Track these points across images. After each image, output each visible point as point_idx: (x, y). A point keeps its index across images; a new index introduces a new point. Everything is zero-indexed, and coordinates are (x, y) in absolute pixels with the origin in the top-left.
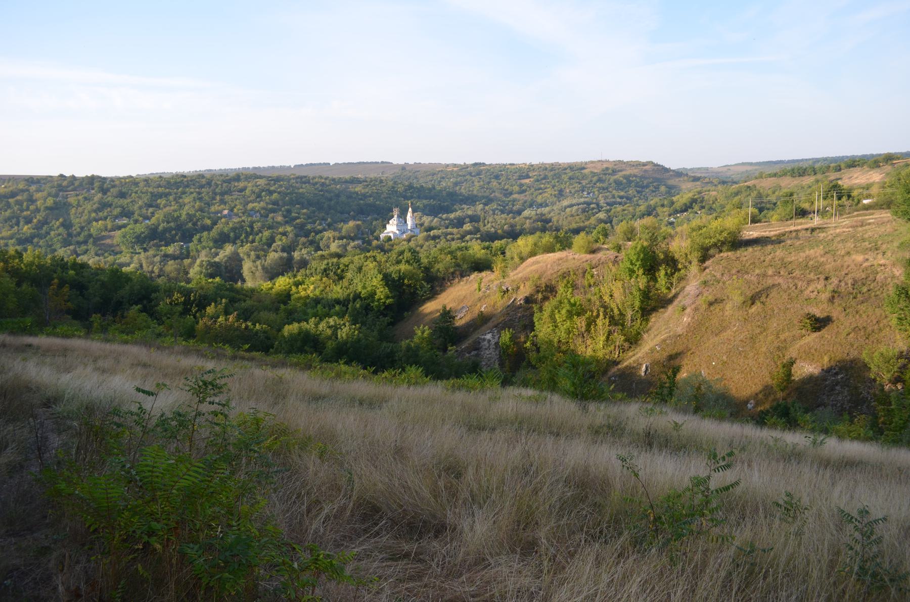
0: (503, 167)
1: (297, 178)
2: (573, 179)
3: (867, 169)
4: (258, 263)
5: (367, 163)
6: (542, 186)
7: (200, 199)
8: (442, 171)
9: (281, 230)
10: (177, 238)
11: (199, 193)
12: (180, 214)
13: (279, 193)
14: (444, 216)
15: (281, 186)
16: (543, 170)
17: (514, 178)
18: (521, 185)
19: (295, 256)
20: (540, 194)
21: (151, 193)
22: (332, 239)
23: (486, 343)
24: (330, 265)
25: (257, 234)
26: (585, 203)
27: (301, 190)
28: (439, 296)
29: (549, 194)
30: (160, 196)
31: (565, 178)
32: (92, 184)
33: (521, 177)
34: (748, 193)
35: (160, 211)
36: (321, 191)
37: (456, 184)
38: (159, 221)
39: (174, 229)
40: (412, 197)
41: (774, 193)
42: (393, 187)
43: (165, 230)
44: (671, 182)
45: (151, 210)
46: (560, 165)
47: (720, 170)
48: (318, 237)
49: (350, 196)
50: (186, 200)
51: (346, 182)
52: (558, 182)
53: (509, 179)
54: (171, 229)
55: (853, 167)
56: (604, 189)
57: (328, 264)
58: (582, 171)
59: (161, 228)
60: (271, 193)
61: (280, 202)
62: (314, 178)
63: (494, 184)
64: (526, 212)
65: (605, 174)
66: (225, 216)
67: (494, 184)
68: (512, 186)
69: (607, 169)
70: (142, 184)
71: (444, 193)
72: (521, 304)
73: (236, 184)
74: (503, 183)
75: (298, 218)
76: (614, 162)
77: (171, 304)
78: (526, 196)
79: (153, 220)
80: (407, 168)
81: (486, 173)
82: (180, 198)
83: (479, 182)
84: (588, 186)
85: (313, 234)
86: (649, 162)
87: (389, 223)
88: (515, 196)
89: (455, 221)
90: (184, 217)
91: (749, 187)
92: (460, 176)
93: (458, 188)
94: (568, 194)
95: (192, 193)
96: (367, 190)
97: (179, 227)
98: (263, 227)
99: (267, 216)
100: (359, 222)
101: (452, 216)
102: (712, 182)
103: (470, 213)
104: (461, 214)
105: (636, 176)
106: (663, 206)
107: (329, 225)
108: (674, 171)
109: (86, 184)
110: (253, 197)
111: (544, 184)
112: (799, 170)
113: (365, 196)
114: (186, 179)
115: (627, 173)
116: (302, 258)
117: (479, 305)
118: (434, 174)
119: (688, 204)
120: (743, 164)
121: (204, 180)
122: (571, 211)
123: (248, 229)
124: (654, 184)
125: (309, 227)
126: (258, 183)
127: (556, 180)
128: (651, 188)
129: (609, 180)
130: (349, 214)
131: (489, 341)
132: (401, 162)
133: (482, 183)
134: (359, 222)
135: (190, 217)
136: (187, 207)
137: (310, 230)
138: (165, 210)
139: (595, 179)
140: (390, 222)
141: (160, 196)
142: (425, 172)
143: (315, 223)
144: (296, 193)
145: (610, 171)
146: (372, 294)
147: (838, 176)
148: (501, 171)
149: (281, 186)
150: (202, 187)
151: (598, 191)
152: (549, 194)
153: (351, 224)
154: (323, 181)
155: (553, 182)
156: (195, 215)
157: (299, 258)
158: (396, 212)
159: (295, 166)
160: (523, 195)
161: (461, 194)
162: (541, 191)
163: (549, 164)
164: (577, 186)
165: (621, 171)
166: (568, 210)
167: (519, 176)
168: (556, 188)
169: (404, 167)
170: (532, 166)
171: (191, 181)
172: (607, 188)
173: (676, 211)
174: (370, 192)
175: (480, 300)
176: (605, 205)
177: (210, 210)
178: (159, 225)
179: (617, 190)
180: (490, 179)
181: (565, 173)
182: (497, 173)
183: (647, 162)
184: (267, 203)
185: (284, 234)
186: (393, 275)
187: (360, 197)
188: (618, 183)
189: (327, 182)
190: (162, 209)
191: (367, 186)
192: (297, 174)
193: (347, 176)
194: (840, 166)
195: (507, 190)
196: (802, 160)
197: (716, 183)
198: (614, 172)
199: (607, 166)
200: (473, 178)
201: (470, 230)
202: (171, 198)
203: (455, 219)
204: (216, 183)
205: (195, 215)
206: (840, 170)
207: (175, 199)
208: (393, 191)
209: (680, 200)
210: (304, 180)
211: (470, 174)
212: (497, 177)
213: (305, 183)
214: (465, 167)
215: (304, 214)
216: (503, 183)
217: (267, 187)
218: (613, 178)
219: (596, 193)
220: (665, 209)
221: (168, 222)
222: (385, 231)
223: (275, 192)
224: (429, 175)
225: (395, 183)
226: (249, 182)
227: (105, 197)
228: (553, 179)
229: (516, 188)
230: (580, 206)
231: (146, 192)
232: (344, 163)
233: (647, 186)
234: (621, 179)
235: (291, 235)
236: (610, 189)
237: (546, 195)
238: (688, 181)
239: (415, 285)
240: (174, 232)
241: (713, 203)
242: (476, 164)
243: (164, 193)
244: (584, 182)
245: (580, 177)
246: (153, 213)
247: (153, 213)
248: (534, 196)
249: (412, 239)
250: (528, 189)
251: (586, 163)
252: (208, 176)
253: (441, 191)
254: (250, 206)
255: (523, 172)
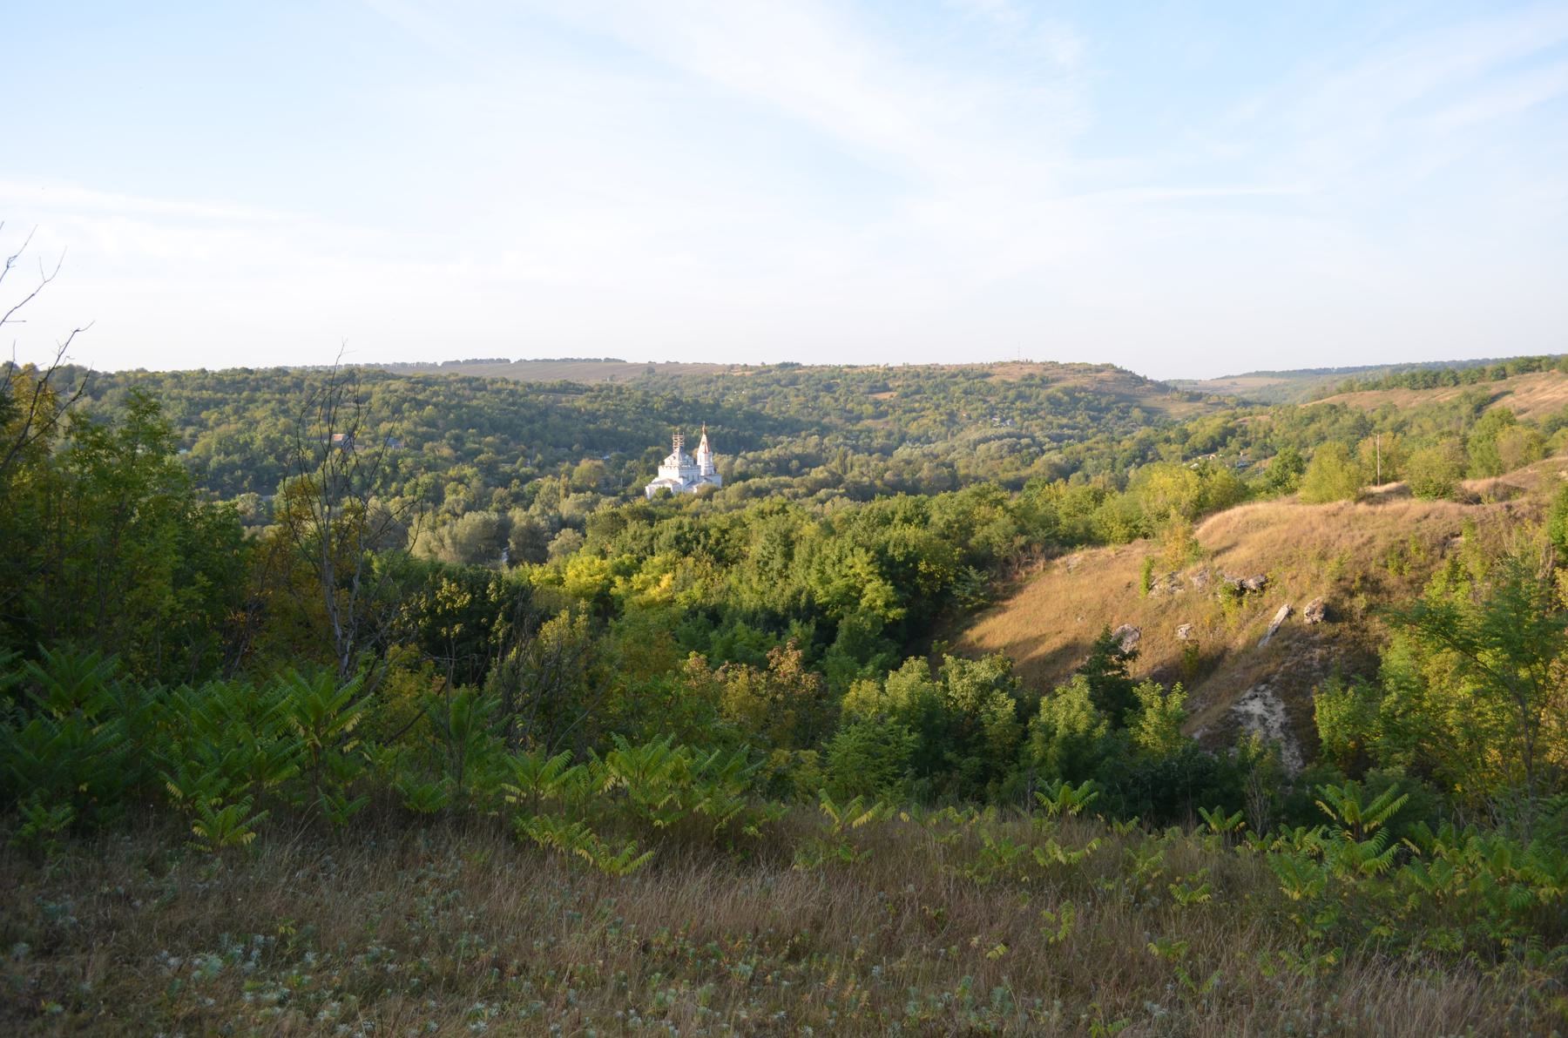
0: (837, 372)
1: (462, 380)
2: (971, 394)
3: (1559, 375)
4: (444, 531)
5: (579, 360)
6: (917, 405)
7: (286, 412)
8: (723, 376)
9: (452, 473)
10: (246, 484)
11: (282, 402)
12: (252, 438)
13: (436, 405)
14: (750, 455)
15: (436, 394)
16: (914, 377)
17: (861, 390)
18: (877, 403)
19: (516, 519)
20: (915, 419)
21: (189, 399)
22: (562, 492)
23: (1255, 724)
24: (686, 529)
25: (406, 480)
26: (1010, 435)
27: (475, 402)
28: (1011, 603)
29: (930, 420)
30: (207, 405)
31: (956, 391)
32: (71, 381)
33: (874, 389)
34: (1333, 418)
35: (209, 432)
36: (513, 404)
37: (754, 400)
38: (208, 450)
39: (241, 467)
40: (680, 421)
41: (1384, 418)
42: (645, 402)
43: (222, 469)
44: (1149, 402)
45: (190, 430)
46: (943, 368)
47: (1218, 384)
48: (527, 487)
49: (567, 415)
50: (259, 414)
51: (553, 390)
52: (944, 398)
53: (852, 392)
54: (231, 468)
55: (1529, 371)
56: (1030, 412)
57: (680, 527)
58: (987, 380)
59: (213, 463)
60: (420, 405)
61: (440, 423)
62: (493, 382)
63: (826, 400)
64: (900, 449)
65: (1030, 386)
66: (338, 445)
67: (826, 400)
68: (860, 404)
69: (1031, 376)
70: (168, 383)
71: (740, 415)
72: (1315, 623)
73: (351, 387)
74: (842, 399)
75: (480, 452)
76: (1043, 364)
77: (431, 611)
78: (887, 422)
79: (198, 449)
80: (658, 371)
81: (807, 380)
82: (246, 410)
83: (797, 396)
84: (1001, 406)
85: (516, 481)
86: (1108, 365)
87: (663, 464)
88: (868, 422)
89: (773, 465)
90: (259, 442)
91: (1333, 407)
92: (760, 385)
93: (758, 406)
94: (965, 421)
95: (267, 401)
96: (596, 406)
97: (249, 464)
98: (417, 465)
99: (420, 448)
100: (599, 463)
101: (766, 455)
102: (1224, 403)
103: (798, 450)
104: (781, 453)
105: (1084, 390)
106: (1168, 440)
107: (540, 466)
108: (1152, 382)
109: (58, 381)
110: (386, 412)
111: (920, 402)
112: (1430, 377)
113: (594, 417)
114: (252, 377)
115: (1070, 384)
116: (530, 523)
117: (1165, 624)
118: (709, 382)
119: (1217, 438)
120: (1258, 374)
121: (288, 379)
122: (989, 449)
123: (388, 470)
124: (1121, 405)
125: (507, 468)
126: (392, 388)
127: (941, 395)
128: (1116, 411)
129: (1037, 397)
130: (570, 449)
131: (1263, 720)
132: (643, 359)
133: (802, 398)
134: (599, 463)
135: (271, 444)
136: (262, 427)
137: (509, 475)
138: (217, 430)
139: (1012, 394)
140: (667, 461)
141: (207, 405)
142: (693, 378)
143: (514, 463)
144: (467, 406)
145: (1037, 381)
146: (851, 597)
147: (1504, 388)
148: (833, 378)
149: (436, 394)
150: (284, 391)
151: (1020, 415)
152: (930, 420)
153: (585, 464)
154: (512, 387)
155: (935, 398)
156: (281, 441)
157: (524, 524)
158: (678, 441)
159: (445, 364)
160: (881, 421)
161: (769, 418)
162: (914, 414)
163: (922, 367)
164: (981, 408)
165: (1058, 380)
166: (982, 447)
167: (871, 387)
168: (942, 410)
169: (651, 369)
170: (891, 369)
171: (264, 379)
172: (1036, 411)
173: (1196, 450)
174: (603, 409)
175: (1163, 612)
176: (1047, 440)
177: (308, 434)
178: (209, 459)
179: (1055, 414)
180: (817, 391)
181: (956, 383)
182: (828, 381)
183: (1103, 365)
184: (416, 424)
185: (460, 480)
186: (890, 551)
187: (586, 417)
188: (1054, 402)
189: (520, 388)
190: (212, 429)
191: (596, 397)
192: (462, 375)
193: (556, 381)
194: (1504, 369)
195: (851, 411)
196: (1363, 368)
197: (1231, 404)
198: (1045, 382)
199: (1030, 371)
200: (785, 390)
201: (825, 479)
202: (228, 409)
203: (772, 460)
204: (311, 385)
205: (281, 441)
206: (1504, 376)
207: (236, 412)
208: (645, 408)
209: (1201, 430)
210: (474, 384)
211: (778, 382)
212: (829, 388)
213: (479, 390)
214: (764, 370)
215: (489, 445)
216: (842, 399)
217: (412, 395)
218: (1044, 393)
219: (1017, 419)
220: (1173, 447)
221: (227, 454)
222: (656, 480)
223: (428, 404)
224: (701, 383)
225: (646, 393)
226: (374, 384)
227: (99, 403)
228: (935, 394)
229: (868, 409)
230: (1005, 441)
231: (178, 398)
232: (536, 361)
233: (1108, 409)
234: (1060, 395)
235: (475, 483)
236: (1042, 413)
237: (925, 421)
238: (1180, 400)
239: (946, 576)
240: (239, 473)
241: (1265, 437)
242: (784, 366)
243: (214, 400)
244: (993, 400)
245: (984, 390)
246: (194, 437)
247: (194, 437)
248: (902, 423)
249: (715, 494)
250: (891, 410)
251: (991, 366)
252: (296, 373)
253: (732, 411)
254: (384, 427)
255: (878, 381)
